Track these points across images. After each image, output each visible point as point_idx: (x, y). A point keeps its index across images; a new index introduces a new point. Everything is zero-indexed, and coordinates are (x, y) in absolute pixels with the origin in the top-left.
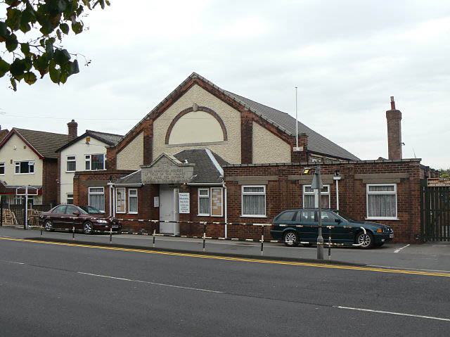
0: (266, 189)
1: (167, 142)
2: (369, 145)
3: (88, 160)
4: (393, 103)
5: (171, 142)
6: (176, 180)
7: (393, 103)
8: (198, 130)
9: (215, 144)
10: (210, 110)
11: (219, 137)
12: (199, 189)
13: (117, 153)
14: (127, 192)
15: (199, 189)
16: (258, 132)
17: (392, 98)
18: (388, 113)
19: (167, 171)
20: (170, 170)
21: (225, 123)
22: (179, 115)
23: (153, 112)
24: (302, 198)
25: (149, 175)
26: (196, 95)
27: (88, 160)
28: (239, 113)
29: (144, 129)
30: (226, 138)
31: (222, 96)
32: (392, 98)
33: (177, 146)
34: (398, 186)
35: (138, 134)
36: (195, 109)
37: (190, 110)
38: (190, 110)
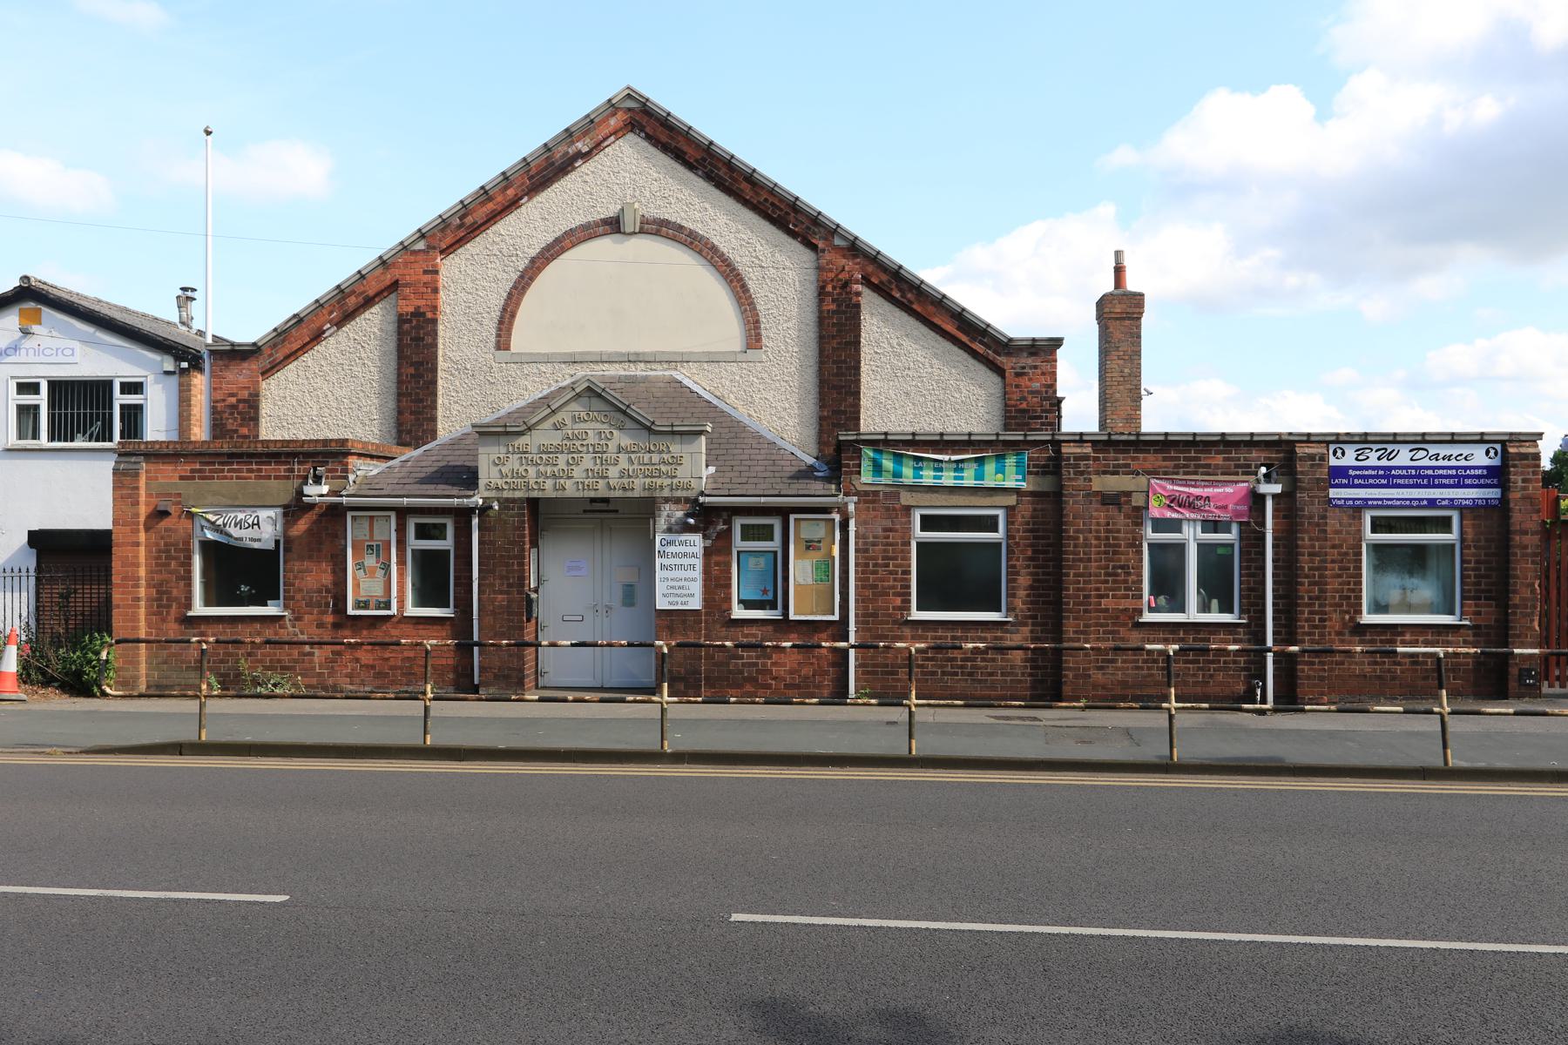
0: (1009, 523)
1: (503, 343)
2: (1059, 395)
3: (29, 399)
4: (1119, 271)
5: (521, 340)
6: (638, 483)
7: (1119, 271)
8: (646, 306)
9: (713, 359)
10: (692, 234)
11: (727, 331)
12: (738, 523)
13: (267, 372)
14: (401, 530)
15: (738, 523)
16: (882, 333)
17: (1118, 254)
18: (1102, 304)
19: (598, 451)
20: (612, 446)
21: (751, 285)
22: (557, 240)
23: (443, 223)
24: (1140, 553)
25: (514, 463)
26: (629, 174)
27: (29, 399)
28: (807, 256)
29: (396, 298)
30: (754, 338)
31: (744, 185)
32: (1118, 254)
33: (548, 359)
34: (1462, 519)
35: (368, 302)
36: (629, 224)
37: (613, 226)
38: (613, 226)
